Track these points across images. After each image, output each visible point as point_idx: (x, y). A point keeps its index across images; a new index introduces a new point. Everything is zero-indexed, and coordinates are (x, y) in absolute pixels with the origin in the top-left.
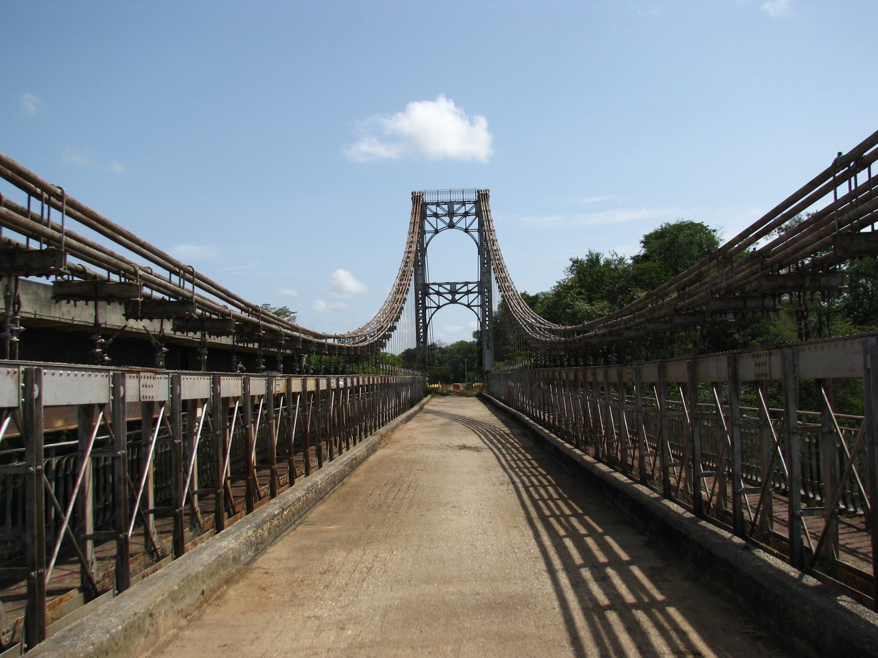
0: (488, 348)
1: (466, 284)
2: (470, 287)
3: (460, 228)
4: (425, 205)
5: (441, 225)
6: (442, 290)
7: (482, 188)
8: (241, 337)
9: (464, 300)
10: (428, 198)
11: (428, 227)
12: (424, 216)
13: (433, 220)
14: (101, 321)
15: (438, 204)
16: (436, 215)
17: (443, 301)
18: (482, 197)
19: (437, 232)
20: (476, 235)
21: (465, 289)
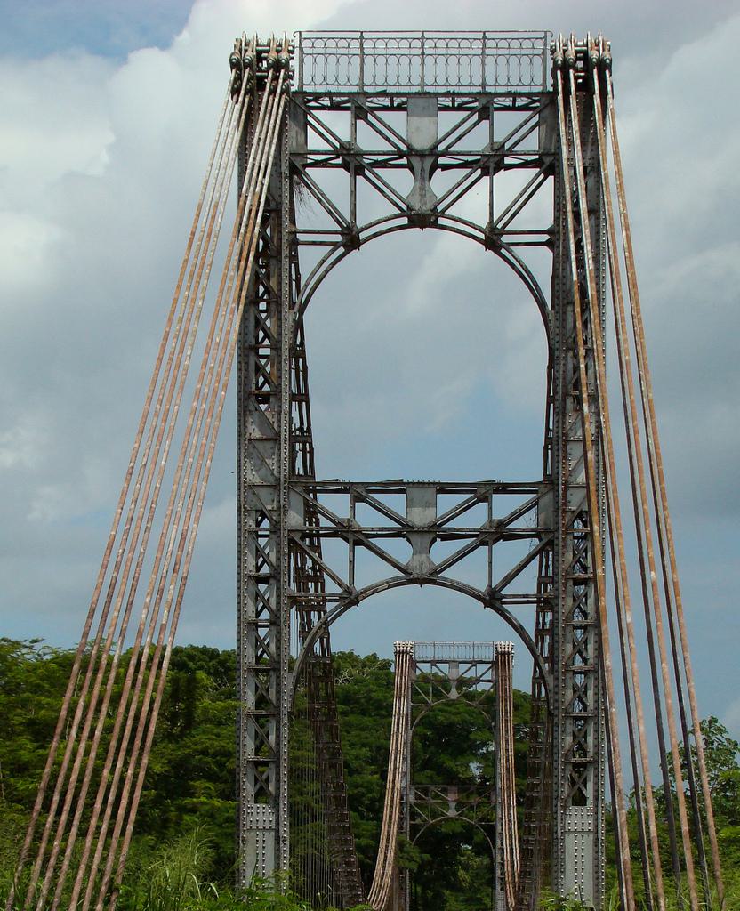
0: (261, 795)
1: (483, 492)
2: (504, 506)
3: (462, 228)
4: (299, 107)
5: (372, 207)
6: (367, 518)
7: (572, 34)
8: (467, 736)
9: (474, 571)
10: (311, 74)
11: (309, 214)
12: (292, 168)
13: (332, 180)
14: (409, 518)
15: (358, 106)
16: (350, 159)
17: (370, 570)
18: (582, 80)
19: (351, 239)
20: (540, 262)
21: (476, 518)
